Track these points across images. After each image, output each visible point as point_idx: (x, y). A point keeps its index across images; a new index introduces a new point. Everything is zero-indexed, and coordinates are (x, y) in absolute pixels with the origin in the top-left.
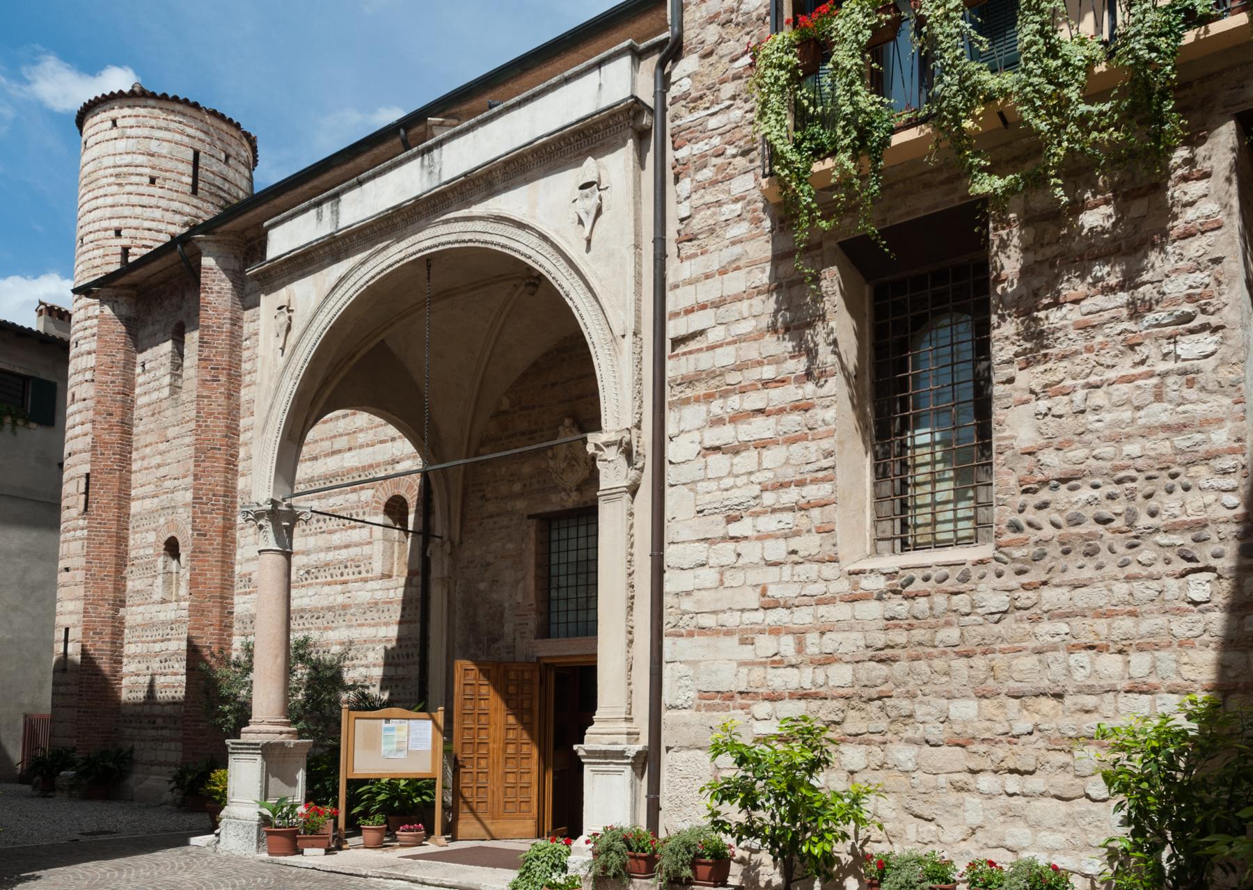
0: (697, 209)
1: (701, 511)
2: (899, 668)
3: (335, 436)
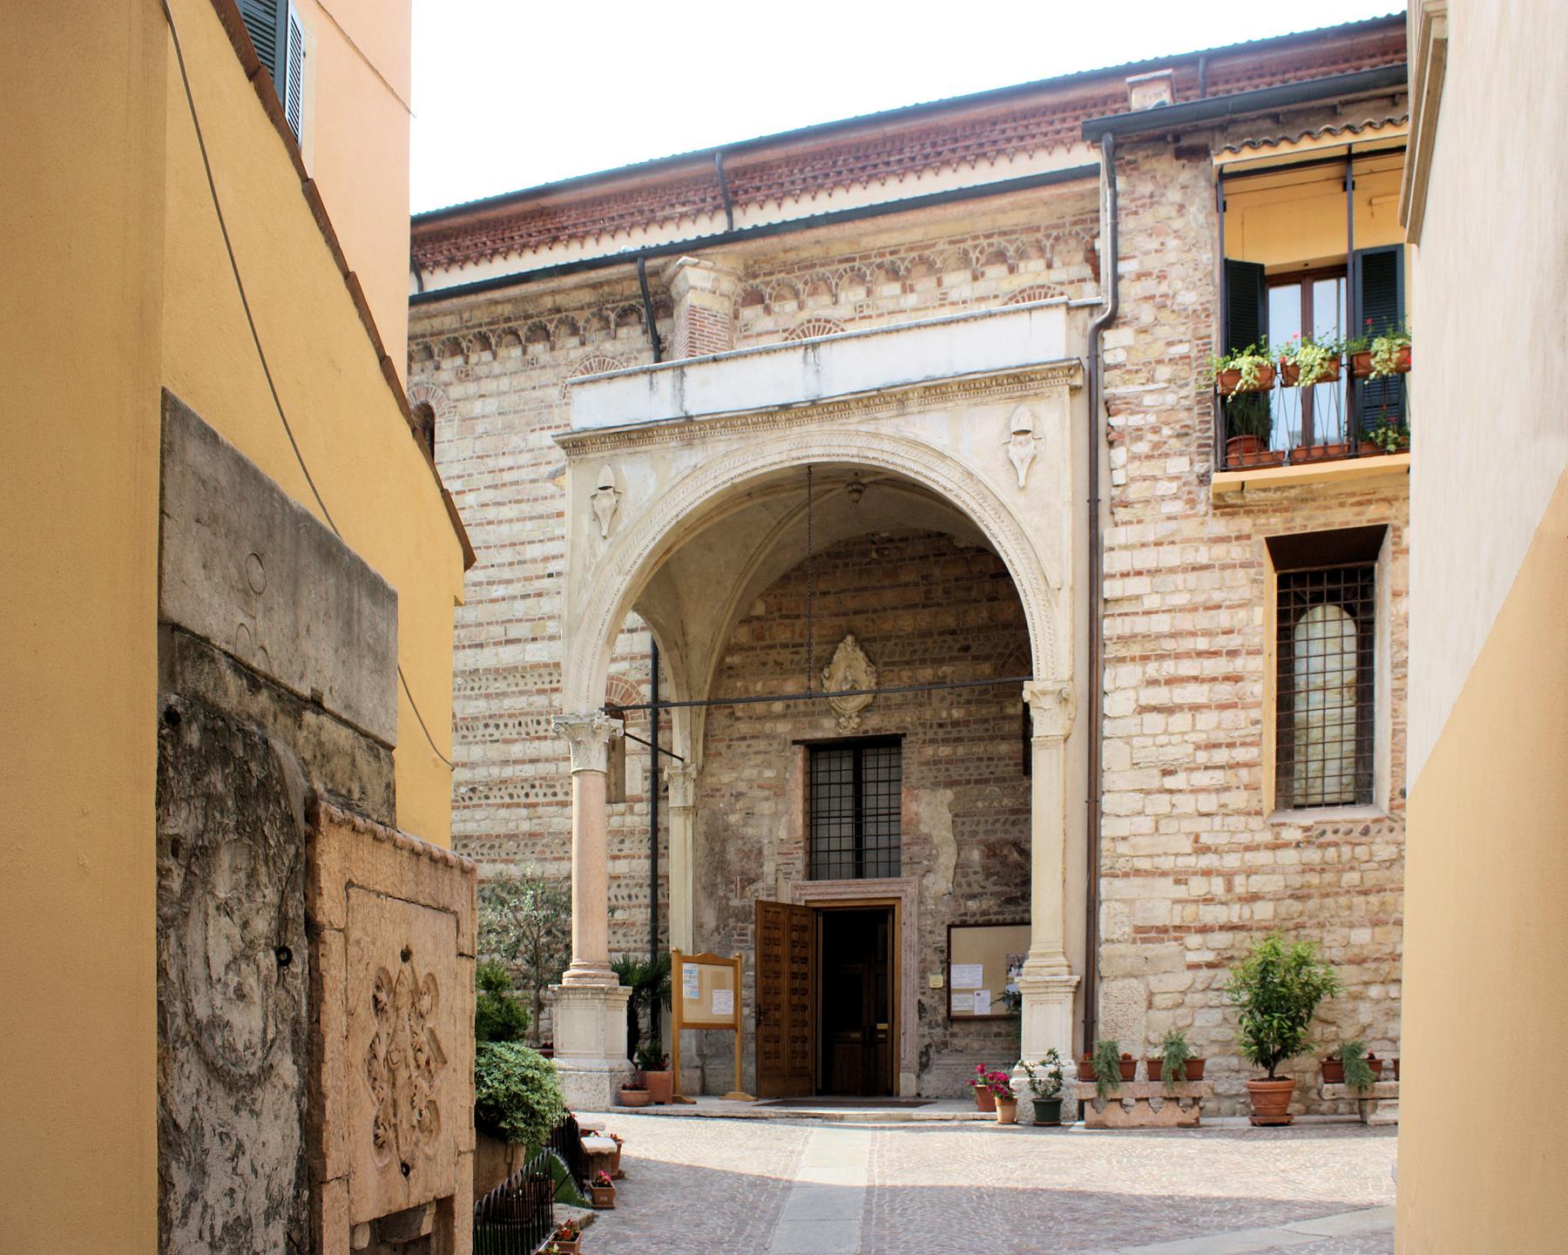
0: (1133, 480)
2: (1312, 904)
3: (510, 621)
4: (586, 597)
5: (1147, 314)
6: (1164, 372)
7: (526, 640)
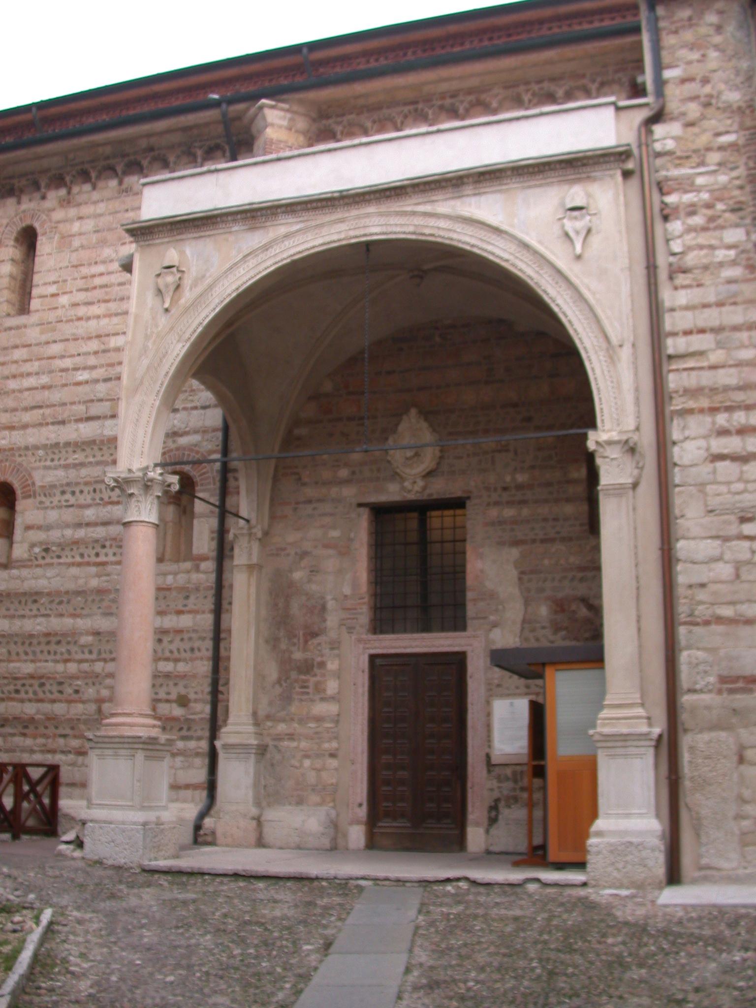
1: (711, 511)
3: (92, 401)
4: (145, 362)
5: (693, 110)
6: (714, 157)
7: (105, 417)
